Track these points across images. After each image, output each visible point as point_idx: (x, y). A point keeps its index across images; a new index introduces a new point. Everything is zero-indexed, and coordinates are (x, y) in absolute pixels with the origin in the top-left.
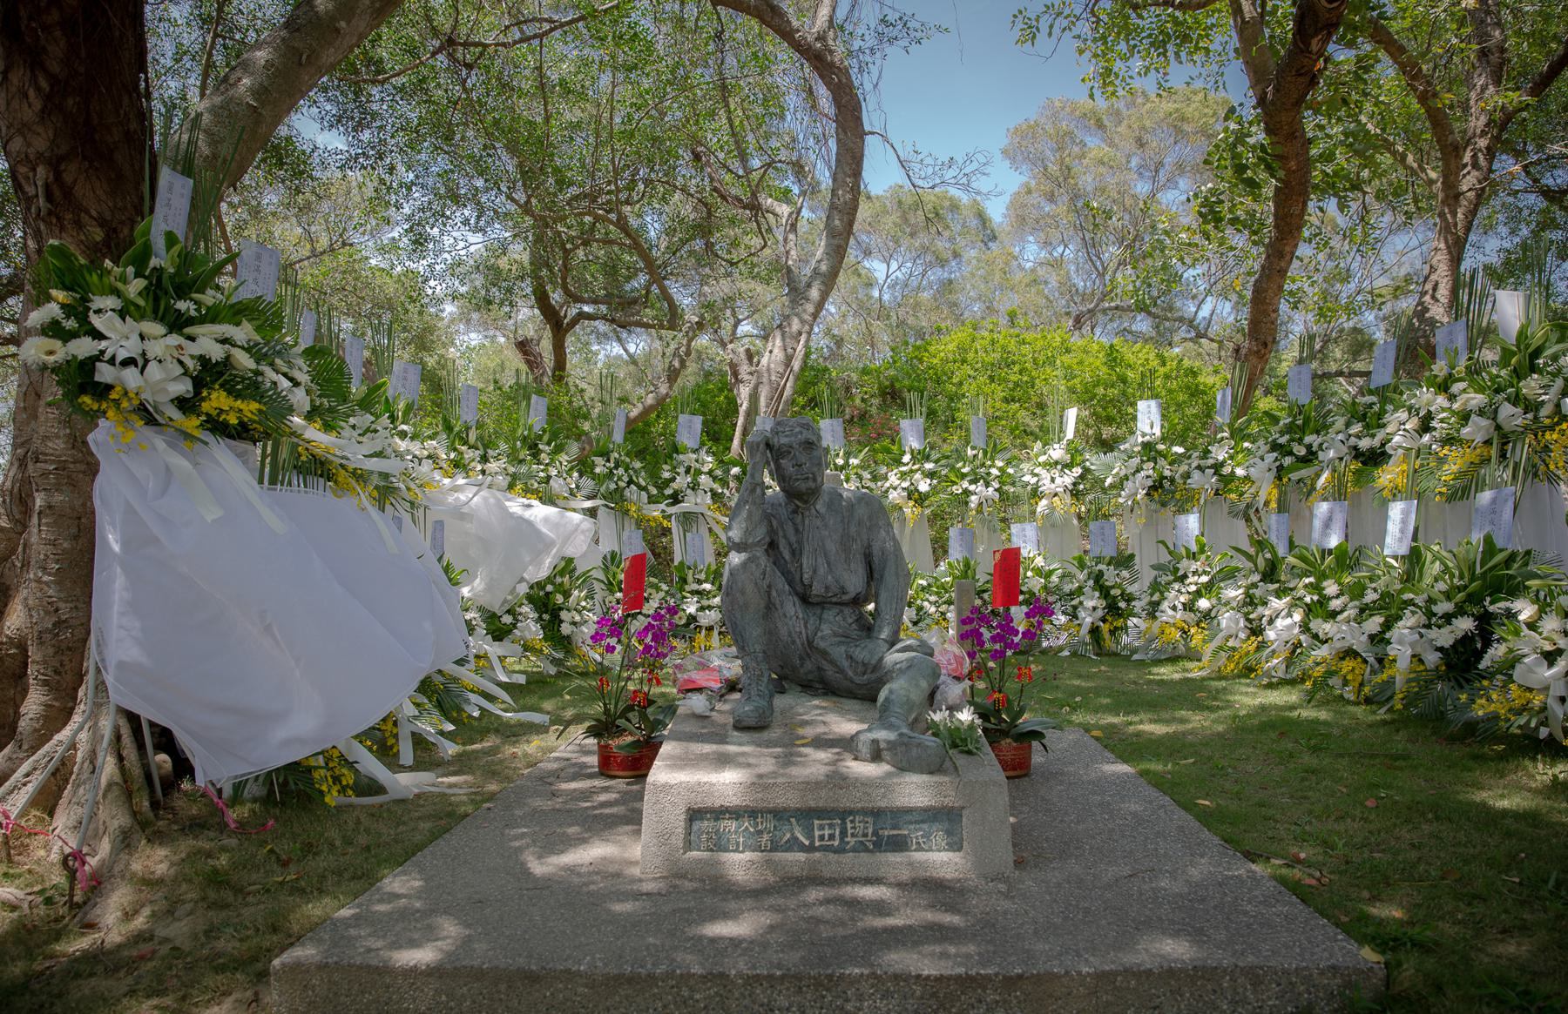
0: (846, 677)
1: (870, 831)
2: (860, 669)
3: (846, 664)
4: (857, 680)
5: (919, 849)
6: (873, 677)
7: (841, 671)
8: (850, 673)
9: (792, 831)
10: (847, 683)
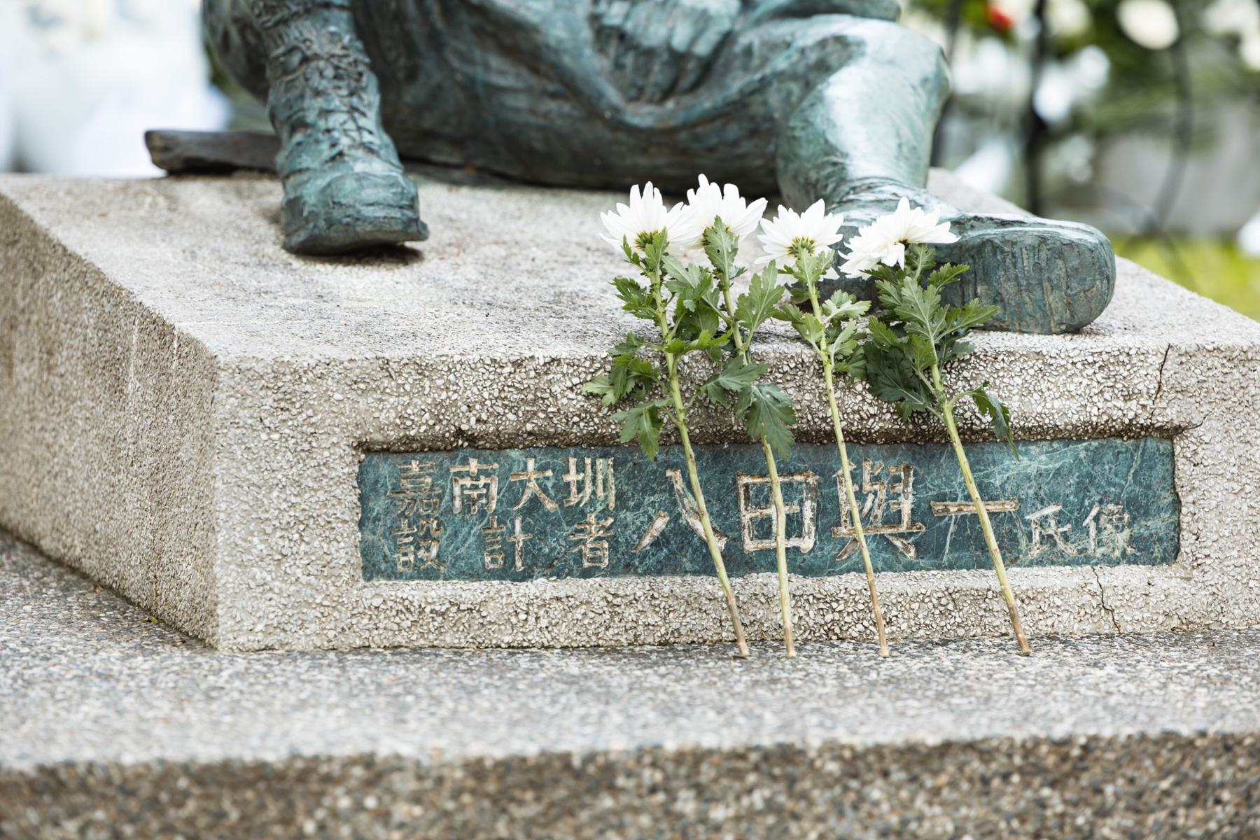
0: (589, 104)
1: (906, 506)
2: (659, 74)
3: (592, 64)
4: (642, 115)
5: (1052, 558)
6: (707, 101)
7: (570, 87)
8: (613, 95)
9: (672, 506)
10: (600, 131)
